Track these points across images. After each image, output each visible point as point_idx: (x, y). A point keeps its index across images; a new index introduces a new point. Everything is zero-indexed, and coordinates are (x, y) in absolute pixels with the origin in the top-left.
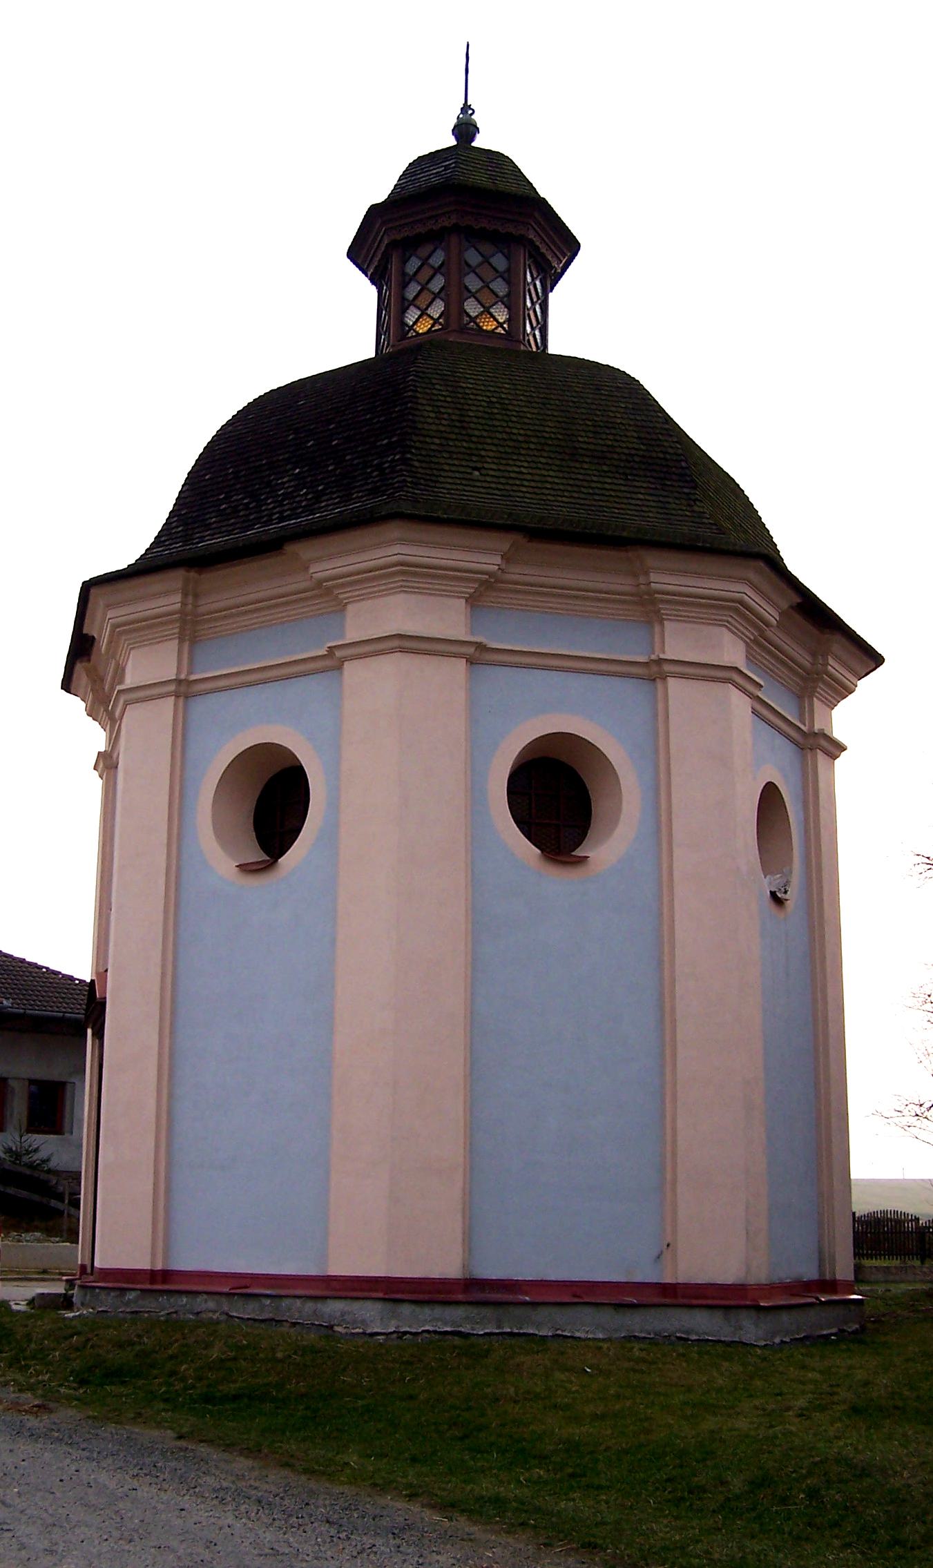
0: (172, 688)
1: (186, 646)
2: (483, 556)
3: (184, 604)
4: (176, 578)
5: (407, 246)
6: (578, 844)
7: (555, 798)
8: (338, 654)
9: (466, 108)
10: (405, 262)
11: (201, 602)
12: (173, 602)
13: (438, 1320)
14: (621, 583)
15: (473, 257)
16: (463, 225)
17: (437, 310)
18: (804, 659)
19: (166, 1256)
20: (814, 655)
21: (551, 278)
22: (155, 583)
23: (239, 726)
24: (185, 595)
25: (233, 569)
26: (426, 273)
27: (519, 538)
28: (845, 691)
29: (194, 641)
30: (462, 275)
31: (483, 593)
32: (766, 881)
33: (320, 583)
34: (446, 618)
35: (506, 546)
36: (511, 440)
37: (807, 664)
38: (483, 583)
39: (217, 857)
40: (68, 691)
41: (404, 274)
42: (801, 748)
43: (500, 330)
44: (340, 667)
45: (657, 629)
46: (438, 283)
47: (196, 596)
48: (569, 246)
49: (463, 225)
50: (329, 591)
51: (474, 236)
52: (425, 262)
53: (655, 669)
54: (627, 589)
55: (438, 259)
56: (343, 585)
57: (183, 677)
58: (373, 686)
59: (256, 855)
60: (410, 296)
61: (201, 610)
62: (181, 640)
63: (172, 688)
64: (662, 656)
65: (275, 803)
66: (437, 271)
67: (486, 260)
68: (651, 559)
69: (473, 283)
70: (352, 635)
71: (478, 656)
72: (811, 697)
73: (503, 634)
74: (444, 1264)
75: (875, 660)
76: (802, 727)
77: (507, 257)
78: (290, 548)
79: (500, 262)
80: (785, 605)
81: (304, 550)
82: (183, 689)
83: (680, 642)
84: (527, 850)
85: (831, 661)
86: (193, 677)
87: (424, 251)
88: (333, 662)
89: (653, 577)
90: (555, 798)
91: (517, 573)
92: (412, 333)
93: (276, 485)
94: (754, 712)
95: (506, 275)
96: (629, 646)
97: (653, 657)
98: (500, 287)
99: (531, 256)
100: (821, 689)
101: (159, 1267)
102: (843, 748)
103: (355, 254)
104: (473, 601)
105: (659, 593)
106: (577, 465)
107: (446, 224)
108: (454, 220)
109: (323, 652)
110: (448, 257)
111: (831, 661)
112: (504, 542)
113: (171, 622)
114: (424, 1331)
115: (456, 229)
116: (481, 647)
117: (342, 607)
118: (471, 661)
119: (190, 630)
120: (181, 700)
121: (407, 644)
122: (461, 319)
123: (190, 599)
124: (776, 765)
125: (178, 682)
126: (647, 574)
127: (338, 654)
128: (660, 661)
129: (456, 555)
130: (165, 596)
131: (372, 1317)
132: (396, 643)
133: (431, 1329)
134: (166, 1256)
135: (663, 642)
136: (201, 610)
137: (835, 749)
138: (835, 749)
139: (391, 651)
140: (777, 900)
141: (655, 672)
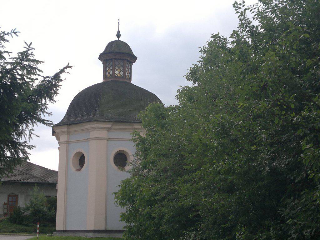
1: (68, 135)
3: (67, 130)
4: (66, 126)
9: (119, 31)
19: (66, 228)
21: (131, 63)
22: (63, 127)
23: (76, 149)
24: (67, 128)
25: (16, 237)
35: (112, 124)
39: (73, 169)
40: (53, 135)
44: (89, 141)
46: (111, 68)
47: (69, 129)
48: (134, 59)
59: (79, 167)
60: (107, 70)
65: (81, 160)
68: (134, 124)
70: (91, 137)
73: (113, 135)
74: (103, 228)
78: (81, 124)
79: (122, 64)
81: (84, 124)
84: (116, 168)
86: (69, 141)
87: (109, 61)
88: (88, 140)
98: (122, 68)
103: (101, 57)
104: (108, 131)
112: (112, 123)
119: (68, 133)
121: (97, 139)
123: (68, 129)
125: (67, 141)
129: (105, 125)
130: (64, 129)
131: (91, 235)
132: (96, 138)
134: (66, 228)
139: (96, 140)
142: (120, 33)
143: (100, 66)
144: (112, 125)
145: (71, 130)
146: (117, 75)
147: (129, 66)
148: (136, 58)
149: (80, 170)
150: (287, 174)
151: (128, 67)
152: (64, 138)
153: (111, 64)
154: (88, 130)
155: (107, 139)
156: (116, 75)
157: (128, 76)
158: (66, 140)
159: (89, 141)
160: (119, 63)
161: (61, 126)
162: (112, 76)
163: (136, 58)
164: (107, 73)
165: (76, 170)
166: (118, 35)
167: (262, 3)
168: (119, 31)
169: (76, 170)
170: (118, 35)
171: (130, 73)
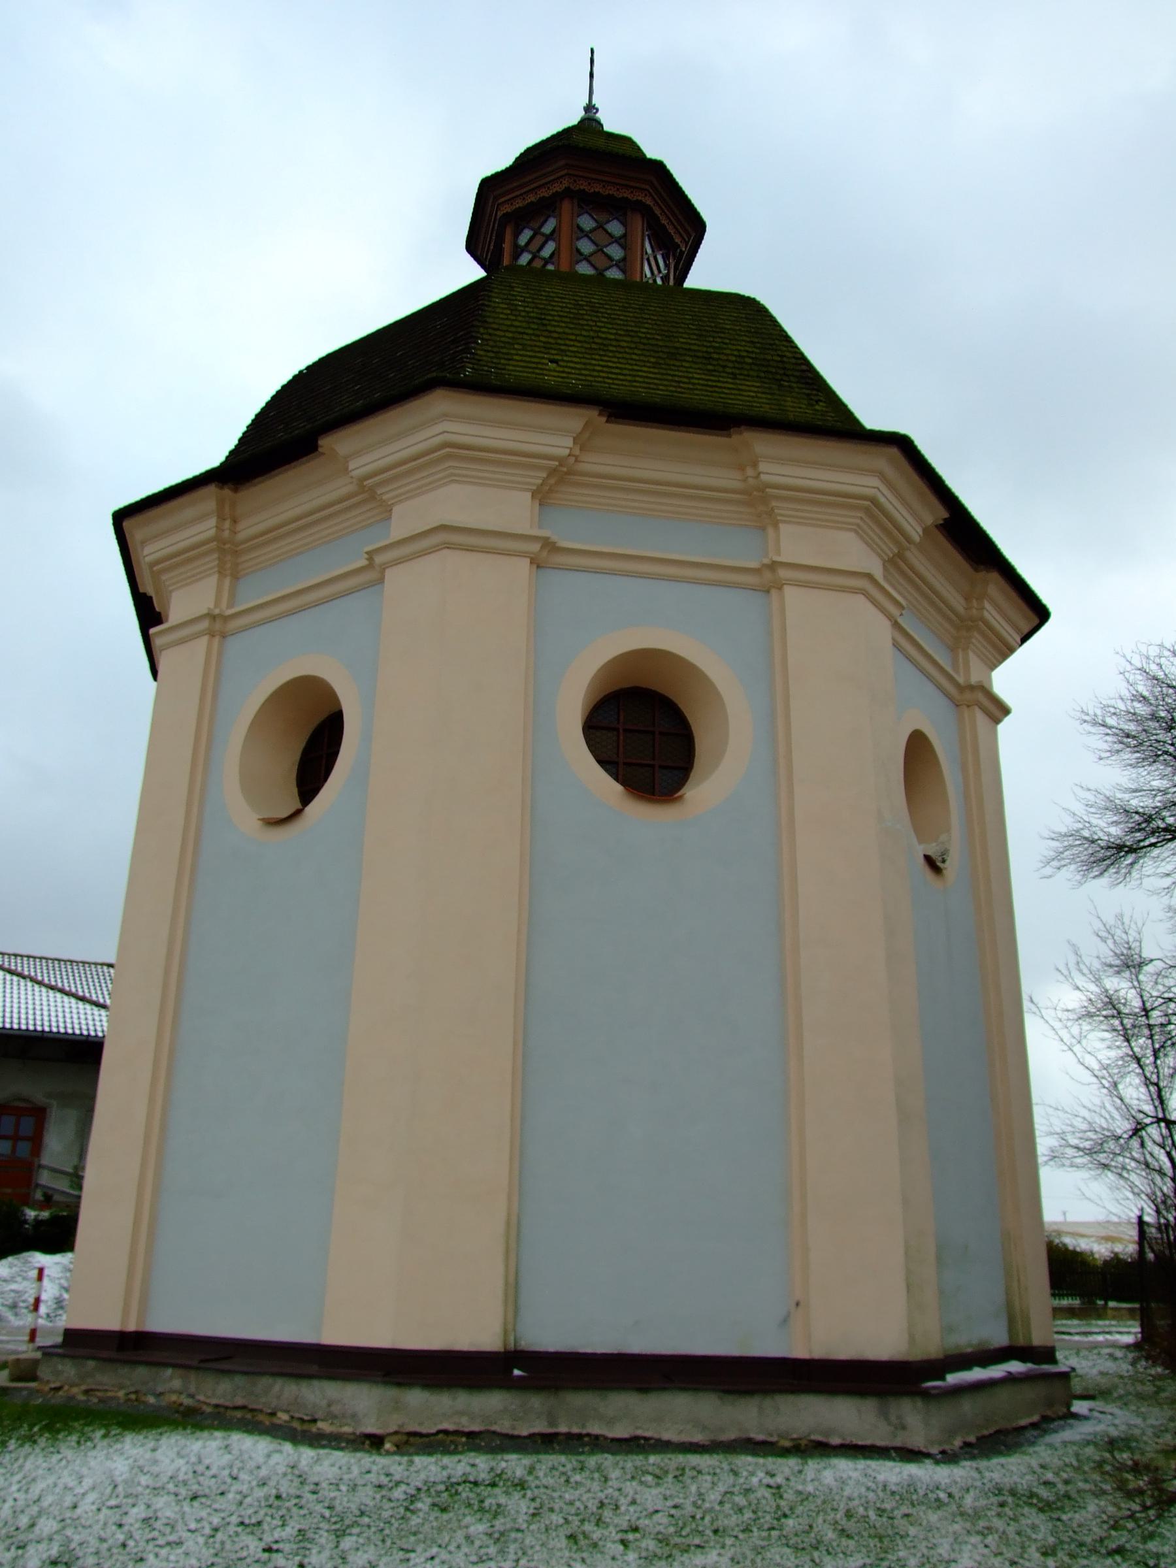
0: (205, 624)
2: (549, 432)
6: (679, 789)
7: (645, 733)
8: (379, 559)
10: (516, 235)
11: (240, 526)
12: (207, 528)
13: (461, 1413)
14: (726, 478)
15: (586, 222)
18: (957, 601)
20: (967, 599)
24: (221, 518)
27: (592, 414)
29: (236, 577)
32: (922, 847)
34: (509, 508)
36: (598, 337)
37: (961, 609)
38: (553, 472)
39: (237, 812)
41: (516, 246)
44: (381, 580)
45: (770, 531)
47: (235, 521)
51: (588, 202)
52: (537, 233)
53: (768, 575)
57: (217, 611)
58: (413, 587)
61: (241, 536)
62: (221, 573)
63: (205, 624)
64: (776, 558)
65: (314, 743)
66: (548, 238)
67: (600, 226)
71: (545, 556)
73: (572, 528)
74: (479, 1333)
76: (955, 676)
77: (624, 224)
80: (929, 520)
82: (218, 626)
83: (796, 543)
85: (987, 605)
88: (372, 573)
89: (763, 467)
90: (645, 733)
91: (597, 463)
94: (896, 644)
95: (622, 241)
96: (739, 549)
97: (766, 561)
99: (650, 227)
100: (977, 639)
101: (132, 1327)
102: (1006, 711)
106: (678, 363)
108: (565, 183)
109: (363, 562)
110: (559, 223)
111: (987, 605)
112: (574, 419)
114: (439, 1432)
115: (568, 193)
116: (549, 546)
118: (537, 563)
119: (230, 557)
120: (217, 640)
123: (227, 524)
124: (928, 714)
125: (212, 617)
126: (755, 465)
127: (379, 559)
128: (773, 566)
133: (451, 1427)
136: (241, 536)
137: (1000, 710)
138: (1000, 710)
140: (933, 864)
141: (769, 579)
154: (371, 497)
155: (535, 547)
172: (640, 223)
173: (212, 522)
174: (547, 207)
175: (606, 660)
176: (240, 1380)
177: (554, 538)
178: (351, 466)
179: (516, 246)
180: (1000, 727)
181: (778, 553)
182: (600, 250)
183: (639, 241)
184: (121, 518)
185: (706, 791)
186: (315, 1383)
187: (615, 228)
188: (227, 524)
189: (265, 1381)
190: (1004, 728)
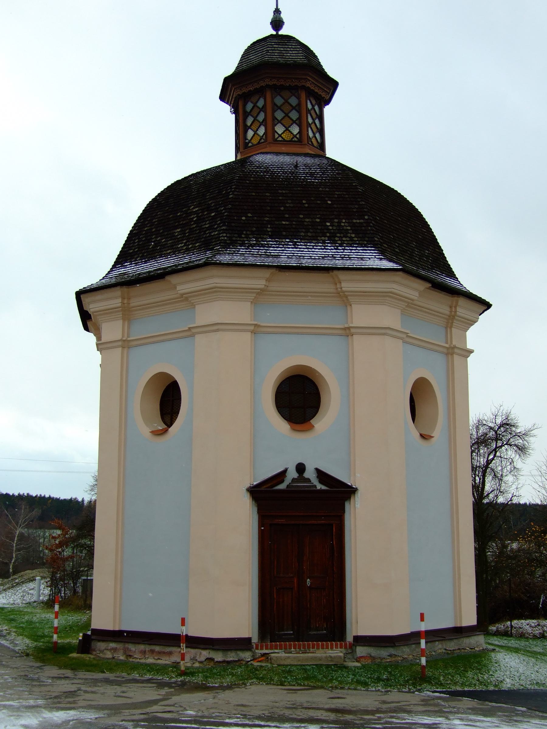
3: (123, 303)
4: (118, 292)
5: (246, 97)
9: (277, 11)
10: (244, 106)
12: (117, 302)
15: (279, 101)
16: (278, 82)
17: (261, 131)
24: (123, 298)
26: (256, 111)
28: (473, 322)
30: (274, 111)
31: (259, 297)
33: (182, 295)
34: (239, 311)
38: (258, 294)
42: (447, 354)
43: (295, 139)
45: (349, 307)
46: (261, 117)
47: (129, 299)
49: (278, 82)
50: (187, 299)
51: (277, 89)
53: (348, 331)
54: (332, 290)
55: (261, 103)
56: (194, 296)
57: (124, 339)
59: (161, 426)
60: (249, 124)
61: (132, 305)
62: (124, 319)
63: (120, 343)
65: (168, 400)
69: (279, 115)
71: (256, 330)
72: (451, 327)
73: (270, 316)
75: (488, 306)
78: (168, 278)
86: (129, 339)
87: (254, 99)
88: (190, 333)
89: (343, 285)
92: (250, 145)
93: (182, 227)
95: (297, 108)
97: (346, 326)
98: (294, 115)
101: (117, 629)
104: (254, 302)
105: (347, 292)
107: (263, 84)
109: (187, 329)
110: (265, 115)
113: (118, 311)
117: (193, 306)
118: (253, 332)
119: (127, 314)
120: (126, 350)
122: (274, 136)
128: (349, 328)
135: (352, 318)
141: (347, 332)
142: (282, 15)
143: (225, 117)
144: (268, 280)
145: (135, 302)
146: (280, 136)
147: (316, 108)
148: (334, 84)
149: (164, 432)
150: (338, 286)
151: (313, 126)
152: (113, 330)
153: (261, 103)
154: (187, 300)
155: (252, 328)
156: (277, 136)
157: (314, 140)
158: (119, 337)
159: (193, 335)
160: (287, 115)
161: (412, 278)
162: (266, 140)
163: (334, 84)
164: (250, 133)
165: (152, 432)
166: (277, 23)
167: (83, 500)
168: (277, 11)
169: (152, 432)
170: (277, 23)
171: (321, 131)
172: (304, 94)
173: (120, 300)
174: (261, 92)
175: (280, 372)
176: (455, 641)
177: (259, 324)
178: (178, 288)
179: (245, 112)
180: (469, 359)
181: (352, 323)
182: (287, 115)
183: (305, 104)
184: (79, 295)
185: (322, 423)
186: (472, 637)
187: (293, 101)
188: (126, 301)
189: (462, 639)
190: (471, 360)
